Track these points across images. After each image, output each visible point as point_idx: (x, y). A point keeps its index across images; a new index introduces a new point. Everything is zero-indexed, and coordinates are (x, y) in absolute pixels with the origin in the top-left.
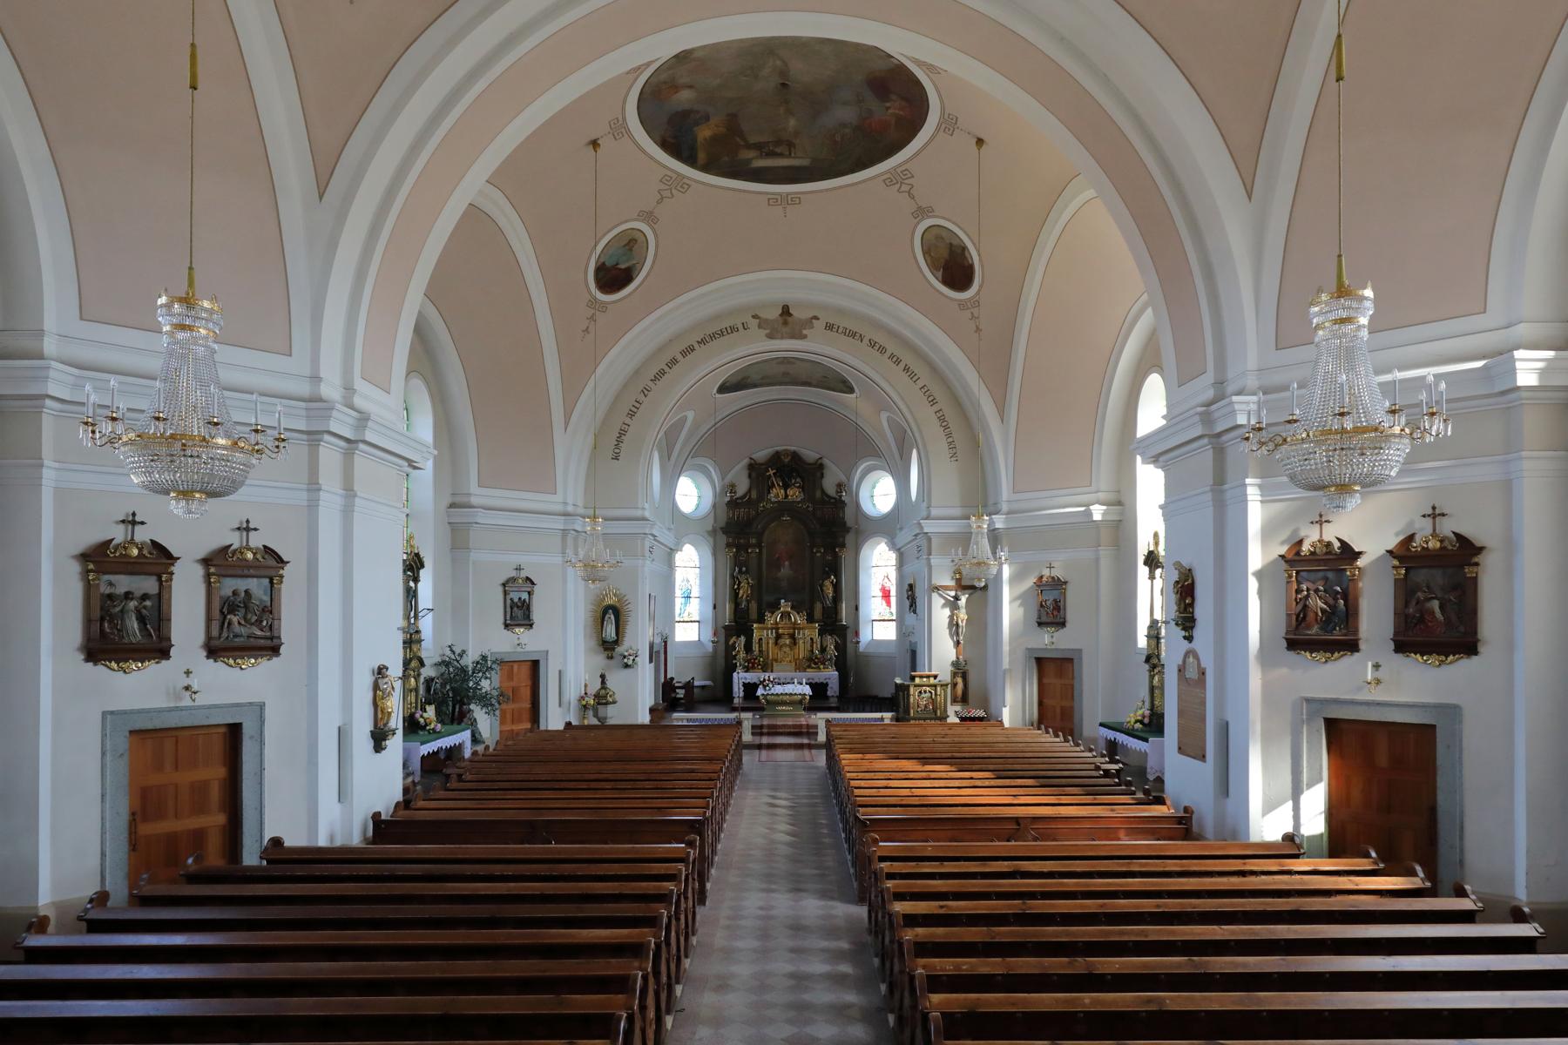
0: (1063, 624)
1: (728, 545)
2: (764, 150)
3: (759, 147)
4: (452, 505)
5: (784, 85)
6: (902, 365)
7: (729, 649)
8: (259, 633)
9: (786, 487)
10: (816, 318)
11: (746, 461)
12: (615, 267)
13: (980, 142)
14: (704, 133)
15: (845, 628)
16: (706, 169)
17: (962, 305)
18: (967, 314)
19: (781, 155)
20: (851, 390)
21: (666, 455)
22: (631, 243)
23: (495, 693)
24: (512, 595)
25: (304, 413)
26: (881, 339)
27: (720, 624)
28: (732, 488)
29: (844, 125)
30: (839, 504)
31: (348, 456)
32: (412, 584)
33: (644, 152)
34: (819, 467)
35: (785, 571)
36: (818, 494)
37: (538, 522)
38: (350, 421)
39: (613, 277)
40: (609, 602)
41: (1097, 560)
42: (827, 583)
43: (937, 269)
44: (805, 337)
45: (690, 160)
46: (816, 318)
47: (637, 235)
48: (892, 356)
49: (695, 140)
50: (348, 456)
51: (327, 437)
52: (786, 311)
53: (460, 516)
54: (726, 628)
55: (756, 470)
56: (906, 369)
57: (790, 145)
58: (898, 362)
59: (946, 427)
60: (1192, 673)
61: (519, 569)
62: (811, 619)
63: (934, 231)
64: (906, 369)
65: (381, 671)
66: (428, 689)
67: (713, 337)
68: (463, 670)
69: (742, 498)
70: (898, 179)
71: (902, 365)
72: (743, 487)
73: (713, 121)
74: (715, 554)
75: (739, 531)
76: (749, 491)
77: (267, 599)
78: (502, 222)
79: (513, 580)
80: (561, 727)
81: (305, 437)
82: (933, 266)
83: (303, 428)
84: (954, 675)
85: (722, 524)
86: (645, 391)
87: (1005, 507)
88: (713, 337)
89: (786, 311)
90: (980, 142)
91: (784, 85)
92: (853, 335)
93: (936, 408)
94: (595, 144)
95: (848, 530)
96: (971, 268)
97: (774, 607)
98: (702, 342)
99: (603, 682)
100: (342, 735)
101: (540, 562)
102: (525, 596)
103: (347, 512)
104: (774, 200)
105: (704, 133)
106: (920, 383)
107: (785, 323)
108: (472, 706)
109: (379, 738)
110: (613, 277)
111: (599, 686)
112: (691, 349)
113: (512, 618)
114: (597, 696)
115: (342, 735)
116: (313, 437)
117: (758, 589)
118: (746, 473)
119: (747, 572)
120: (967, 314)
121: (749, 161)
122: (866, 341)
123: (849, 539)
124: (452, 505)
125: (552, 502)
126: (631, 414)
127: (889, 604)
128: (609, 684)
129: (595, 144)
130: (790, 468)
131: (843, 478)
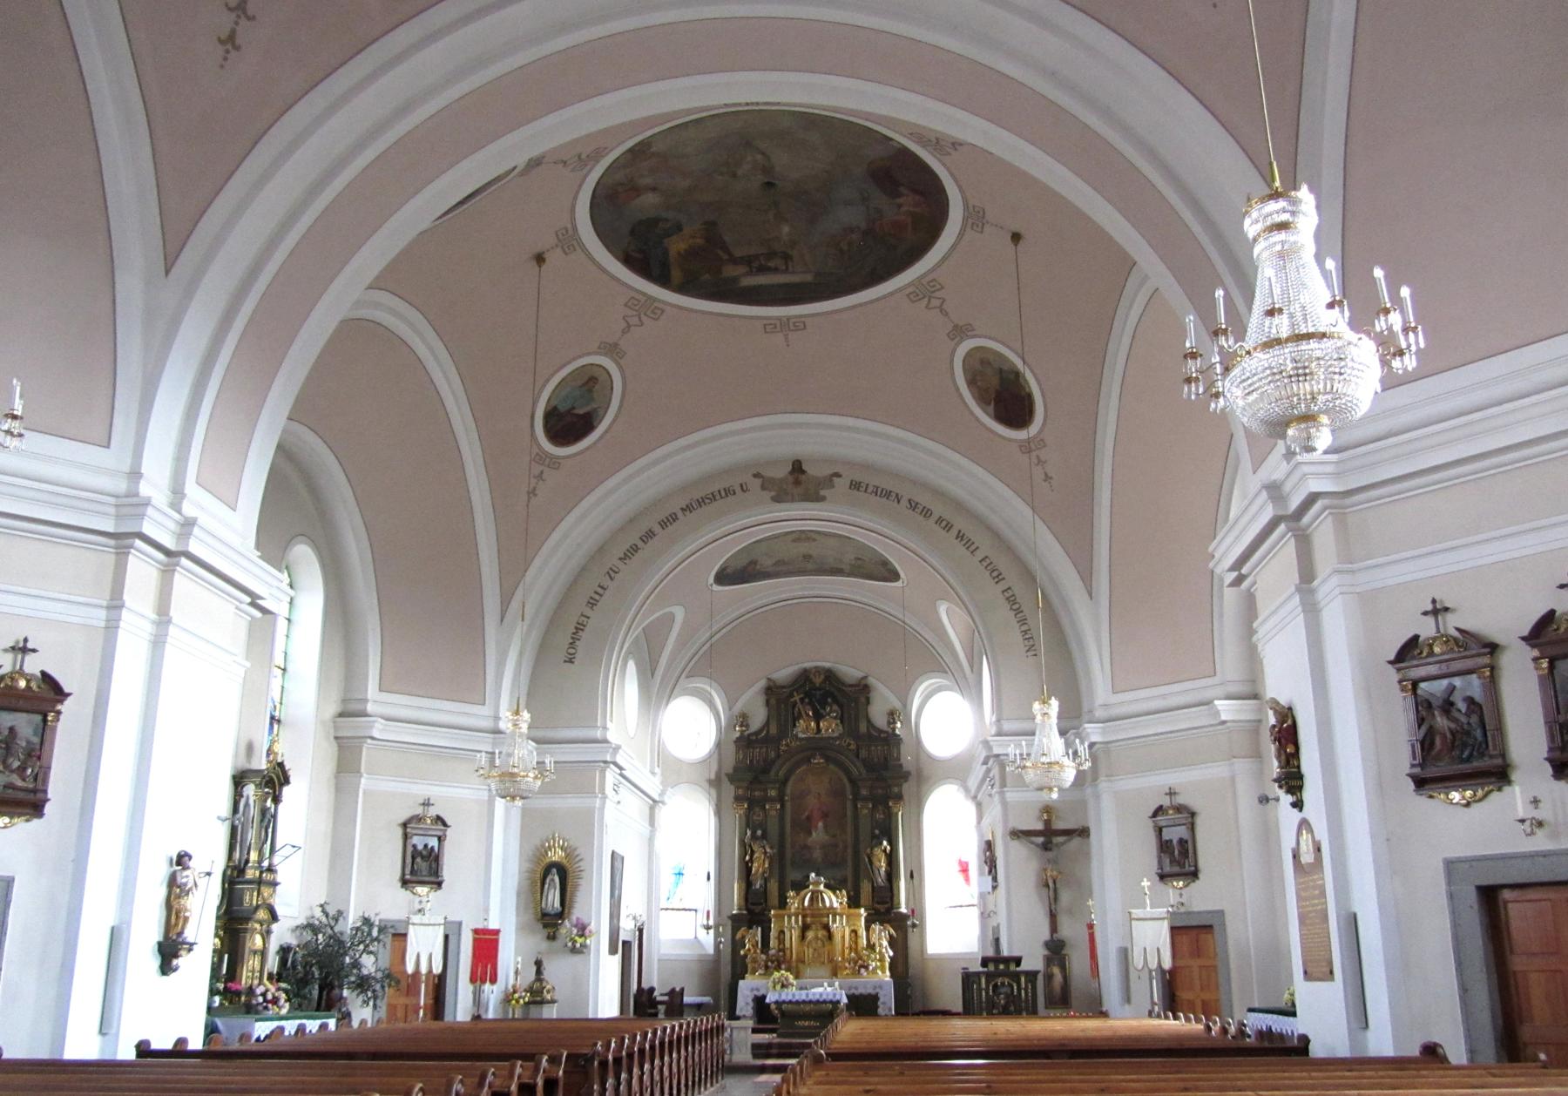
0: (1194, 875)
1: (738, 799)
3: (748, 261)
4: (341, 715)
5: (769, 185)
6: (954, 532)
7: (737, 945)
8: (19, 783)
9: (818, 717)
10: (838, 475)
11: (762, 683)
12: (569, 411)
13: (1016, 237)
14: (677, 246)
15: (905, 917)
16: (682, 289)
19: (776, 270)
20: (893, 576)
21: (647, 673)
22: (591, 383)
23: (379, 975)
24: (416, 840)
25: (112, 510)
26: (924, 499)
27: (726, 913)
28: (744, 719)
29: (852, 230)
30: (889, 740)
31: (167, 573)
32: (269, 803)
34: (862, 690)
35: (818, 835)
36: (863, 728)
37: (460, 752)
38: (172, 526)
39: (568, 424)
40: (556, 855)
41: (1233, 779)
42: (877, 851)
44: (823, 499)
45: (663, 280)
46: (838, 475)
48: (940, 520)
49: (666, 252)
50: (167, 573)
51: (138, 543)
52: (797, 467)
53: (350, 727)
54: (734, 918)
55: (774, 694)
56: (960, 536)
57: (787, 258)
58: (948, 527)
59: (1018, 611)
60: (1307, 857)
61: (427, 804)
62: (854, 902)
64: (960, 536)
65: (182, 860)
66: (283, 962)
67: (701, 502)
68: (336, 941)
69: (757, 733)
70: (925, 291)
71: (954, 532)
72: (758, 717)
73: (687, 231)
74: (719, 812)
75: (755, 777)
76: (767, 724)
77: (36, 740)
78: (422, 351)
79: (418, 819)
80: (468, 1019)
81: (112, 542)
82: (982, 399)
83: (111, 530)
84: (1048, 961)
85: (729, 766)
86: (612, 573)
87: (1099, 713)
88: (701, 502)
90: (1016, 237)
91: (769, 185)
92: (887, 494)
93: (1003, 585)
95: (906, 776)
96: (1030, 396)
97: (800, 886)
98: (688, 509)
99: (539, 972)
100: (116, 939)
101: (458, 795)
102: (433, 842)
103: (158, 643)
104: (771, 326)
105: (677, 246)
106: (980, 555)
107: (797, 483)
108: (346, 993)
109: (169, 951)
110: (568, 424)
111: (532, 976)
112: (673, 518)
113: (413, 872)
114: (530, 990)
115: (116, 939)
116: (122, 541)
117: (779, 862)
118: (761, 700)
119: (764, 836)
121: (735, 280)
122: (904, 502)
123: (907, 789)
124: (341, 715)
125: (477, 715)
126: (592, 603)
127: (967, 879)
128: (546, 975)
129: (540, 259)
130: (824, 692)
131: (897, 705)
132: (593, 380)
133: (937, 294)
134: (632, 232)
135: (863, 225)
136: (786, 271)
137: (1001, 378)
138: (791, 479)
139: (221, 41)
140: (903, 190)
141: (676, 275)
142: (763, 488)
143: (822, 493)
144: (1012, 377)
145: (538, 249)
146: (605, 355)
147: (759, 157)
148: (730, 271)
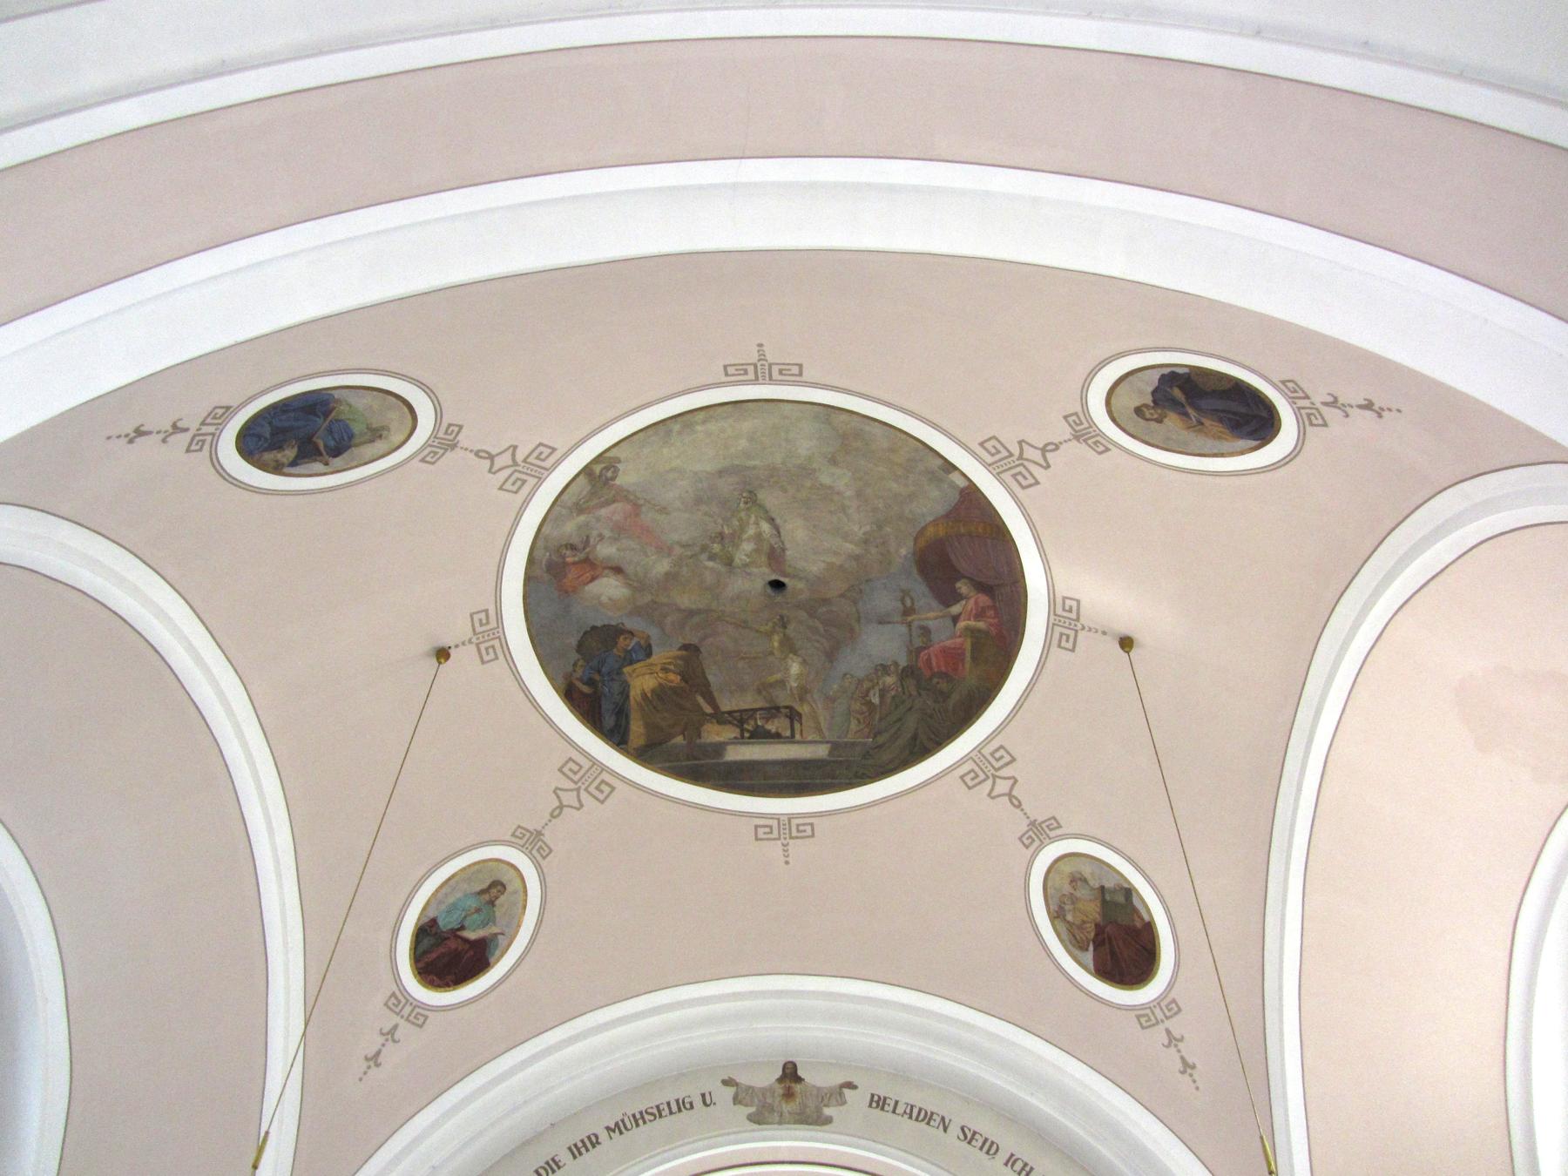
2: (750, 727)
3: (739, 719)
5: (777, 585)
10: (850, 1086)
12: (454, 933)
13: (1126, 643)
14: (642, 681)
16: (643, 756)
17: (1145, 1017)
18: (1159, 1035)
22: (494, 890)
26: (985, 1126)
29: (884, 669)
33: (537, 707)
39: (450, 954)
43: (1084, 949)
44: (828, 1121)
45: (616, 736)
46: (850, 1086)
47: (506, 876)
49: (625, 692)
52: (790, 1074)
57: (793, 716)
63: (1067, 868)
67: (639, 1119)
70: (988, 768)
73: (660, 656)
82: (1074, 943)
88: (639, 1119)
89: (790, 1074)
90: (1126, 643)
92: (927, 1117)
94: (442, 654)
96: (1149, 928)
98: (617, 1128)
104: (766, 829)
105: (642, 681)
107: (789, 1095)
110: (450, 954)
120: (1159, 1035)
121: (719, 749)
122: (954, 1130)
129: (442, 654)
132: (498, 886)
133: (1004, 772)
134: (580, 647)
135: (903, 663)
136: (791, 739)
137: (1104, 902)
138: (779, 1090)
139: (367, 1059)
140: (963, 587)
141: (637, 731)
142: (736, 1100)
143: (827, 1111)
144: (1121, 899)
145: (445, 641)
146: (521, 848)
147: (765, 527)
148: (715, 734)
